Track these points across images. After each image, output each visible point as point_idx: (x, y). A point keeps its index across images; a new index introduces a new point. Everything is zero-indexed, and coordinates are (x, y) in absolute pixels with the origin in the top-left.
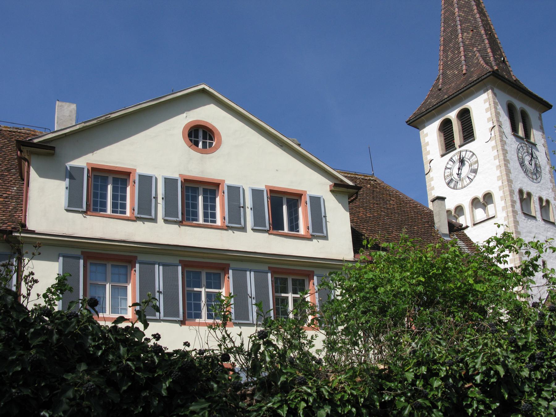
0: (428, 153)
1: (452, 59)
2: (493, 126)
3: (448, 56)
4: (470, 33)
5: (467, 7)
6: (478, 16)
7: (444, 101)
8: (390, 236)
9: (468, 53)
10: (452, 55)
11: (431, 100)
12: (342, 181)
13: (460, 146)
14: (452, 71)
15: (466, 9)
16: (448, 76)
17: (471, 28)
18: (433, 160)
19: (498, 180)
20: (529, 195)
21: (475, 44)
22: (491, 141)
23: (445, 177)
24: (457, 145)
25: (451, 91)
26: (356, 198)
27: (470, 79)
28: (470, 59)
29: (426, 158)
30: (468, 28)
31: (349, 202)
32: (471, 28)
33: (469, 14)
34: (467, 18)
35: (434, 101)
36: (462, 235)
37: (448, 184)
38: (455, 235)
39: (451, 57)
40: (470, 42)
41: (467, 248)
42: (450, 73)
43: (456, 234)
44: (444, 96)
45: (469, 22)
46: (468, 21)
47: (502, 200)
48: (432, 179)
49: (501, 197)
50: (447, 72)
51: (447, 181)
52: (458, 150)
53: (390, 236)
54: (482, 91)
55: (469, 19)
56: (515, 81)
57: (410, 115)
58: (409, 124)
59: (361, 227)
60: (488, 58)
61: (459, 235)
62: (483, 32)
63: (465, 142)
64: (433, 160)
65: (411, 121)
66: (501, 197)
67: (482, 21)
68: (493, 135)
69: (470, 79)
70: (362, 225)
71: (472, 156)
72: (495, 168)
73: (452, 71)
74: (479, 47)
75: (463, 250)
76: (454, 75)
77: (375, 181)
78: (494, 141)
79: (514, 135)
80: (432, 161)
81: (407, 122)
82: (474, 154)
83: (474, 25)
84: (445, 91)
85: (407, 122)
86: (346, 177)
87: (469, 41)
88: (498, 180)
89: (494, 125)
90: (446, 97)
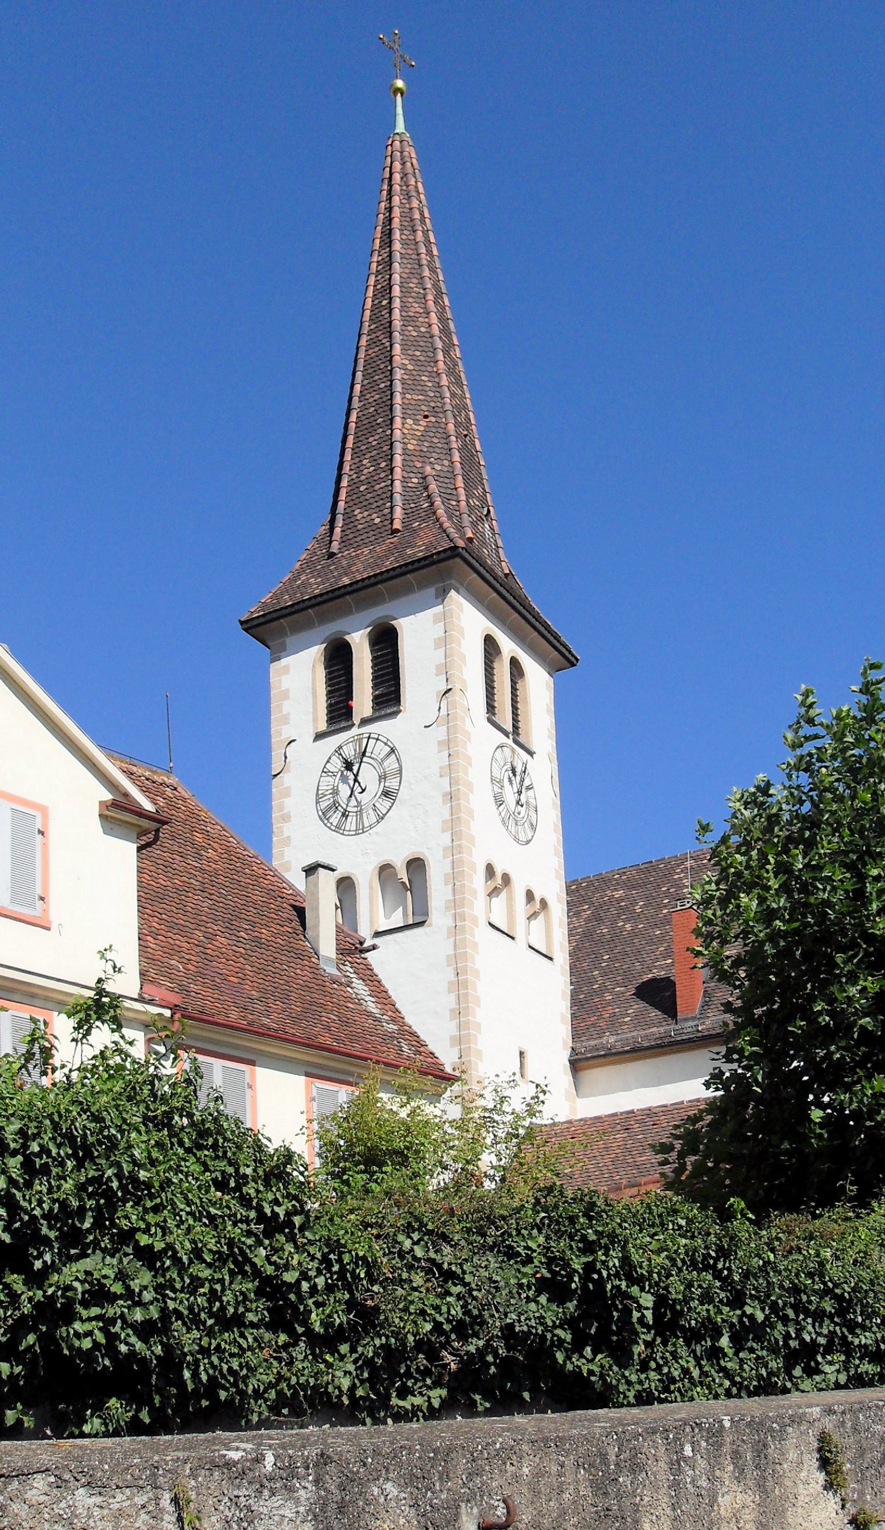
0: (286, 719)
1: (370, 482)
2: (445, 688)
3: (361, 468)
4: (421, 423)
5: (421, 349)
6: (444, 381)
7: (337, 593)
8: (210, 946)
9: (412, 475)
10: (372, 468)
11: (308, 579)
12: (126, 795)
13: (365, 722)
14: (366, 513)
15: (418, 353)
16: (356, 523)
17: (423, 407)
18: (294, 740)
19: (443, 831)
20: (506, 878)
21: (428, 455)
22: (438, 726)
23: (317, 794)
24: (356, 720)
25: (361, 572)
26: (155, 841)
27: (409, 552)
28: (412, 494)
29: (280, 732)
30: (418, 408)
31: (139, 849)
32: (423, 407)
33: (423, 368)
34: (418, 378)
35: (317, 587)
36: (362, 966)
37: (324, 816)
38: (347, 963)
39: (369, 475)
40: (418, 448)
41: (373, 999)
42: (361, 515)
43: (350, 962)
44: (340, 577)
45: (423, 392)
46: (419, 388)
47: (446, 884)
48: (287, 793)
49: (446, 875)
50: (356, 513)
51: (324, 805)
52: (355, 731)
53: (210, 946)
54: (431, 591)
55: (422, 383)
56: (506, 575)
57: (253, 610)
58: (246, 630)
59: (147, 910)
60: (454, 503)
61: (355, 965)
62: (451, 427)
63: (377, 714)
64: (294, 740)
65: (255, 623)
66: (446, 875)
67: (453, 395)
68: (444, 712)
69: (409, 552)
70: (150, 907)
71: (388, 755)
72: (440, 799)
73: (366, 513)
74: (438, 467)
75: (364, 1003)
76: (371, 526)
77: (175, 789)
78: (445, 728)
79: (490, 721)
80: (292, 744)
81: (242, 623)
82: (393, 750)
83: (433, 404)
84: (344, 563)
85: (242, 623)
86: (130, 774)
87: (415, 442)
88: (443, 831)
89: (449, 687)
90: (346, 581)
